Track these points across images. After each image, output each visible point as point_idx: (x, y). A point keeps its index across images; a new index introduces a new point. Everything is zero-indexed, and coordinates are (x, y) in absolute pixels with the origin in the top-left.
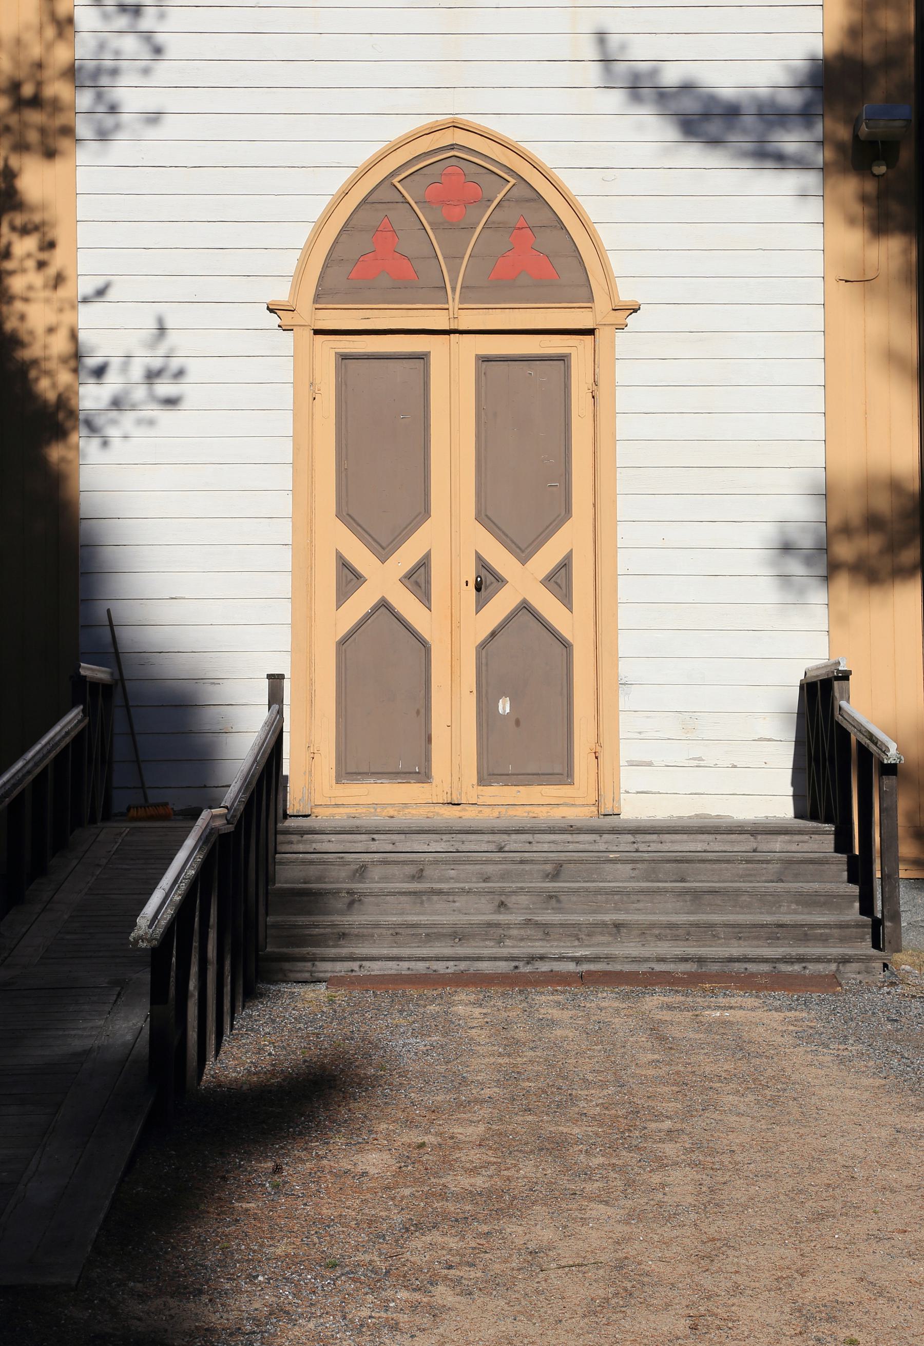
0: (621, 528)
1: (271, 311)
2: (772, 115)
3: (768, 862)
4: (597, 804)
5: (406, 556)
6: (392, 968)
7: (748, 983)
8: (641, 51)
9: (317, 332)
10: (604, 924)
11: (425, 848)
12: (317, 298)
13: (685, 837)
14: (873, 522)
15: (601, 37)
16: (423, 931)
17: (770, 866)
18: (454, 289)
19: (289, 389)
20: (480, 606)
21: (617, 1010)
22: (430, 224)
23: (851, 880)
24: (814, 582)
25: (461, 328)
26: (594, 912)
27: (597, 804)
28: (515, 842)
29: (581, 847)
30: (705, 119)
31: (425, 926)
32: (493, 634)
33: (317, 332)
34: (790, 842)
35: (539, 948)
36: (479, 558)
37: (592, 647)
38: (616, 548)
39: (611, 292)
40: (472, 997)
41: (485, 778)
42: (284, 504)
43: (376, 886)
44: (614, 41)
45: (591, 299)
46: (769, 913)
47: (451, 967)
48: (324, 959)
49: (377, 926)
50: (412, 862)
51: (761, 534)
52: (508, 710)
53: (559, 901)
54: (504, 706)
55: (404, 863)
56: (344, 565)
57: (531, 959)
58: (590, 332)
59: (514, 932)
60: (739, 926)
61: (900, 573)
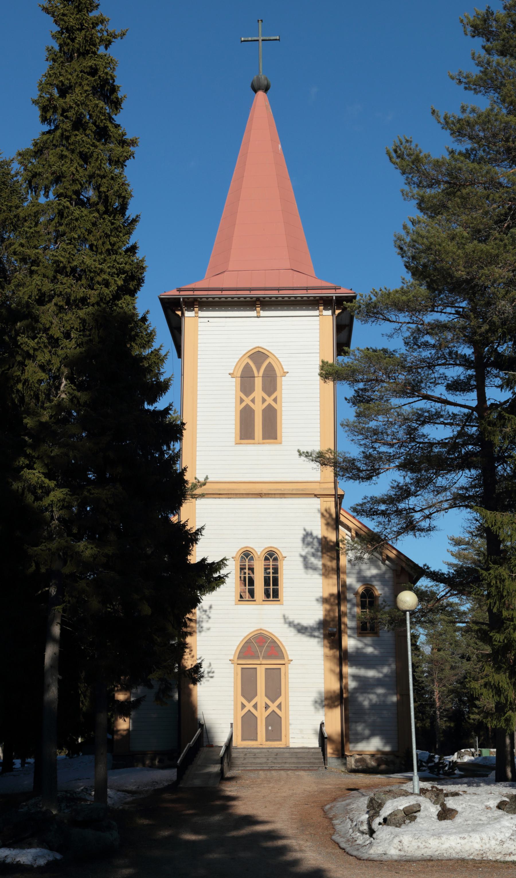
2: (313, 629)
5: (253, 703)
8: (291, 618)
15: (284, 616)
20: (266, 711)
28: (270, 750)
30: (302, 630)
39: (288, 658)
41: (267, 740)
42: (232, 693)
44: (286, 616)
54: (270, 728)
56: (242, 704)
61: (336, 706)
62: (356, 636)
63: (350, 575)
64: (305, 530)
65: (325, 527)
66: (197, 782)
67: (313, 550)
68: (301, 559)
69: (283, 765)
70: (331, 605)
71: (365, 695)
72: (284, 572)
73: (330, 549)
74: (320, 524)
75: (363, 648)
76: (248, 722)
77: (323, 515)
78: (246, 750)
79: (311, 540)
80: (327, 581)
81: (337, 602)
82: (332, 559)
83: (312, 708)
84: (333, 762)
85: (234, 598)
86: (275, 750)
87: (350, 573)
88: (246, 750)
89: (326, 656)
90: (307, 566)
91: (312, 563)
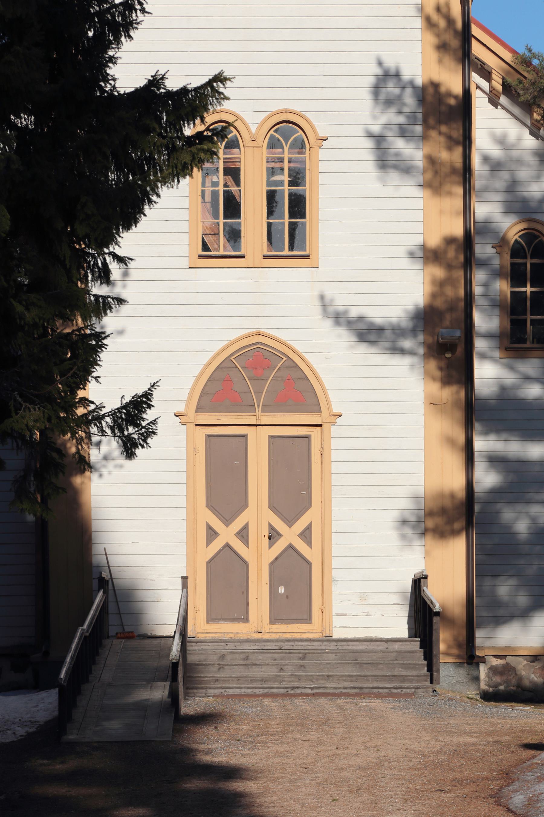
0: (333, 512)
1: (177, 416)
2: (398, 331)
3: (391, 652)
4: (322, 632)
5: (237, 525)
6: (238, 692)
7: (379, 696)
8: (341, 302)
9: (197, 425)
10: (323, 676)
11: (249, 648)
12: (197, 410)
13: (358, 643)
14: (443, 511)
15: (322, 297)
16: (250, 679)
17: (392, 654)
18: (258, 406)
19: (185, 451)
20: (270, 546)
21: (327, 704)
22: (248, 377)
23: (424, 659)
24: (415, 536)
25: (262, 424)
26: (319, 672)
27: (322, 632)
28: (286, 646)
29: (314, 647)
30: (369, 333)
31: (250, 677)
32: (276, 559)
33: (197, 425)
34: (402, 645)
35: (296, 684)
36: (270, 525)
37: (320, 564)
38: (331, 521)
39: (329, 408)
40: (271, 700)
41: (273, 620)
42: (183, 501)
43: (229, 663)
44: (328, 297)
45: (320, 411)
46: (390, 672)
47: (262, 691)
48: (210, 688)
49: (231, 677)
50: (244, 653)
51: (394, 515)
52: (283, 592)
53: (305, 668)
54: (281, 590)
55: (240, 653)
56: (209, 528)
57: (293, 688)
58: (320, 425)
59: (287, 679)
60: (377, 676)
61: (455, 533)
62: (497, 354)
63: (487, 195)
64: (380, 64)
65: (433, 55)
66: (115, 727)
67: (401, 119)
68: (369, 144)
69: (322, 683)
70: (449, 267)
71: (520, 507)
72: (322, 179)
73: (445, 115)
74: (418, 47)
75: (515, 387)
76: (225, 576)
77: (429, 23)
78: (222, 646)
79: (397, 91)
80: (436, 203)
81: (462, 258)
82: (451, 142)
83: (394, 539)
84: (449, 672)
85: (186, 250)
86: (299, 646)
87: (485, 189)
88: (222, 646)
89: (434, 404)
90: (386, 161)
91: (397, 154)
